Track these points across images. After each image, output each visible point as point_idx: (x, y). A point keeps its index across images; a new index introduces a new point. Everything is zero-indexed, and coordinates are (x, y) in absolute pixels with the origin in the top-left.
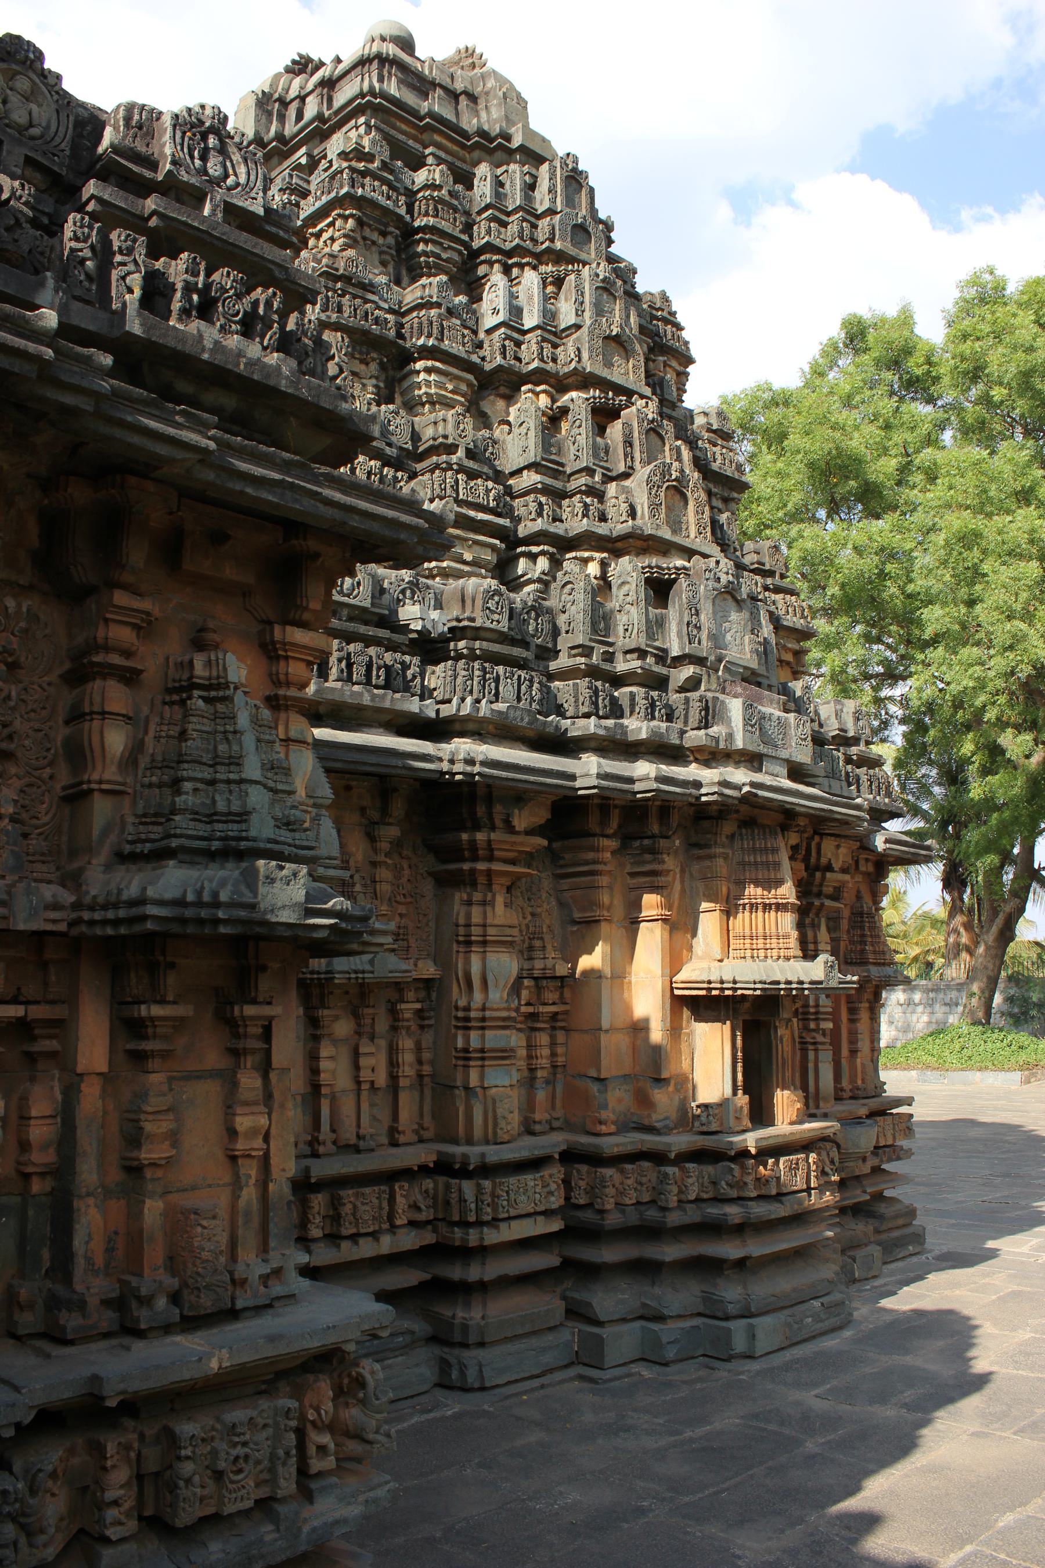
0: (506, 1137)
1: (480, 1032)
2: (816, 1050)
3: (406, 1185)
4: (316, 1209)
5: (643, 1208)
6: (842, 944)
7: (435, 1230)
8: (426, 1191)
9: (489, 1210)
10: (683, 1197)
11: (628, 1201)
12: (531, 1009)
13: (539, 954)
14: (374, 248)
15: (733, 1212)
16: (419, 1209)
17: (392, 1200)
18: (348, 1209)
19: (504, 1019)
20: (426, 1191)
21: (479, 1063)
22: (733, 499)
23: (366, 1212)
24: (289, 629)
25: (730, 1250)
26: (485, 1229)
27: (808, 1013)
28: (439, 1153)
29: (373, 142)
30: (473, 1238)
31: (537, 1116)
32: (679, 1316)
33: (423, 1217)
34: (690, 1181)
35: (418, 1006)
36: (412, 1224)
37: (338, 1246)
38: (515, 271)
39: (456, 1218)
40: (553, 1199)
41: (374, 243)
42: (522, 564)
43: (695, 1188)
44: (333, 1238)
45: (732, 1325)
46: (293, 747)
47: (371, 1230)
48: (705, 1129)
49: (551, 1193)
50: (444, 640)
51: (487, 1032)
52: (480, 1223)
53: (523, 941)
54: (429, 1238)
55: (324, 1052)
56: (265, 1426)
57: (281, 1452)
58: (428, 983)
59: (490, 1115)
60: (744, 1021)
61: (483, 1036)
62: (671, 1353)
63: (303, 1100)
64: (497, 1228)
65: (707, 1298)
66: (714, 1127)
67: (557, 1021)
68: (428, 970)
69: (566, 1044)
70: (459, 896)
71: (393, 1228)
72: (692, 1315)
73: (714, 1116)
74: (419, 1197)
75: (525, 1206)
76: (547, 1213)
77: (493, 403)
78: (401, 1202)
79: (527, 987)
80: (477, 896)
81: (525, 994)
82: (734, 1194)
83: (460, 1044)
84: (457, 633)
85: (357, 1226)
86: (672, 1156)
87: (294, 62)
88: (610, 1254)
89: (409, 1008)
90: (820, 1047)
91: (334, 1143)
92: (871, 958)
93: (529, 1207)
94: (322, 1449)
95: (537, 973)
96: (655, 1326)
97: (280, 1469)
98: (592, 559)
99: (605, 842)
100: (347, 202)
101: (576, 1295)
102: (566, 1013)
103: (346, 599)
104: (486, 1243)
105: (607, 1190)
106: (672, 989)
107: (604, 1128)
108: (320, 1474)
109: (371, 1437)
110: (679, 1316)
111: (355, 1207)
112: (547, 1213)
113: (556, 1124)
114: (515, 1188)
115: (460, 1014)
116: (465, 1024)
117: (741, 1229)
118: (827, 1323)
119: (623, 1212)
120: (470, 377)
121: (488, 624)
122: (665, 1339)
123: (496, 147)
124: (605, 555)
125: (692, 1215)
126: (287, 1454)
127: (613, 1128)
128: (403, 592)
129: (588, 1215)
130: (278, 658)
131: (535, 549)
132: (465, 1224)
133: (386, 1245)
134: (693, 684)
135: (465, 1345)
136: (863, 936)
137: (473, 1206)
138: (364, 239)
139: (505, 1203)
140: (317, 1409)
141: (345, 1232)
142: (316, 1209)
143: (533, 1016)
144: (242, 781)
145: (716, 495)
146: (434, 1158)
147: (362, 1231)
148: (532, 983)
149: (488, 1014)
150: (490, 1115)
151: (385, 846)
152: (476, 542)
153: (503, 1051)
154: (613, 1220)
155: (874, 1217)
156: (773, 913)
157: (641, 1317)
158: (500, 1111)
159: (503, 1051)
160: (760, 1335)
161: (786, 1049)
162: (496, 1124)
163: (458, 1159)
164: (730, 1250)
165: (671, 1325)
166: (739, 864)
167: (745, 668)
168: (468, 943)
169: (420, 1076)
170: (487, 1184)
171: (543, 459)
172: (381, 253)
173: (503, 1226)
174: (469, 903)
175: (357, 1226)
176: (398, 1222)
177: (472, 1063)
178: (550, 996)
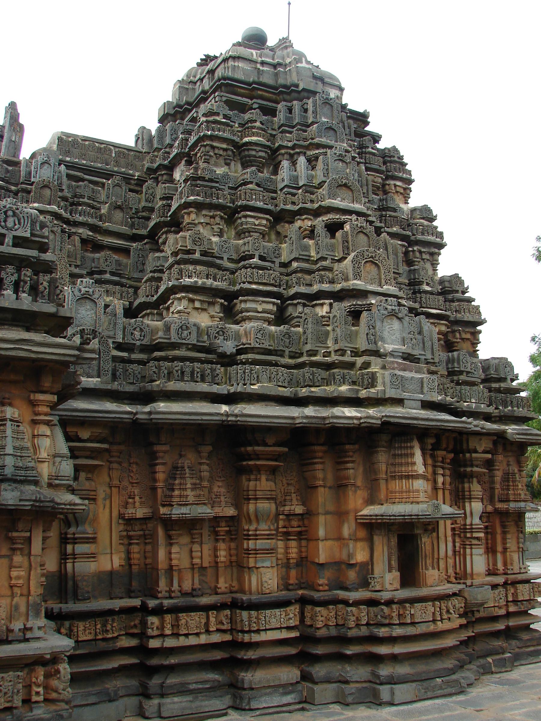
0: (268, 591)
1: (254, 541)
2: (471, 548)
3: (215, 612)
4: (168, 621)
5: (339, 627)
6: (496, 491)
7: (232, 634)
8: (227, 615)
9: (255, 625)
10: (359, 622)
11: (331, 624)
12: (285, 530)
13: (288, 503)
14: (221, 158)
15: (383, 632)
16: (223, 624)
17: (208, 618)
18: (183, 622)
19: (268, 535)
20: (227, 615)
21: (254, 556)
22: (436, 253)
23: (192, 624)
24: (37, 395)
25: (383, 650)
26: (252, 634)
27: (466, 529)
28: (233, 598)
29: (218, 107)
30: (247, 638)
31: (291, 582)
32: (357, 682)
33: (224, 627)
34: (363, 614)
35: (227, 529)
36: (218, 630)
37: (178, 639)
38: (295, 157)
39: (239, 628)
40: (291, 621)
41: (221, 155)
42: (290, 310)
43: (366, 618)
44: (176, 635)
45: (381, 687)
46: (41, 438)
47: (195, 632)
48: (373, 589)
49: (291, 619)
50: (232, 356)
51: (258, 541)
52: (249, 632)
53: (282, 497)
54: (228, 637)
55: (173, 550)
56: (10, 681)
57: (16, 691)
58: (232, 518)
59: (260, 580)
60: (398, 535)
61: (256, 543)
62: (350, 699)
63: (166, 572)
64: (259, 633)
65: (374, 674)
66: (377, 588)
67: (302, 535)
68: (231, 512)
69: (307, 547)
70: (244, 478)
71: (208, 632)
72: (365, 682)
73: (378, 582)
74: (224, 619)
75: (274, 623)
76: (289, 628)
77: (283, 227)
78: (212, 619)
79: (282, 519)
80: (252, 477)
81: (281, 523)
82: (387, 621)
83: (245, 546)
84: (240, 352)
85: (188, 630)
86: (351, 602)
87: (201, 60)
88: (320, 650)
89: (223, 528)
90: (473, 547)
91: (180, 591)
92: (511, 497)
93: (276, 626)
94: (38, 693)
95: (286, 512)
96: (343, 686)
97: (15, 697)
98: (325, 304)
99: (317, 448)
100: (205, 139)
101: (307, 669)
102: (306, 531)
103: (184, 341)
104: (252, 641)
105: (317, 618)
106: (356, 519)
107: (321, 588)
108: (36, 702)
109: (61, 691)
110: (357, 682)
111: (187, 621)
112: (289, 628)
113: (303, 586)
114: (269, 615)
115: (245, 533)
116: (248, 537)
117: (392, 640)
118: (445, 690)
119: (328, 629)
120: (268, 217)
121: (257, 346)
122: (347, 693)
123: (290, 92)
124: (332, 301)
125: (364, 631)
126: (18, 691)
127: (326, 588)
128: (218, 333)
129: (309, 630)
130: (35, 405)
131: (295, 302)
132: (243, 632)
133: (203, 639)
134: (366, 365)
135: (245, 689)
136: (508, 486)
137: (247, 623)
138: (216, 154)
139: (263, 622)
140: (37, 679)
141: (181, 633)
142: (168, 621)
143: (287, 534)
144: (5, 455)
145: (424, 252)
146: (230, 600)
147: (190, 632)
148: (284, 517)
149: (474, 527)
150: (260, 580)
151: (205, 454)
152: (263, 302)
153: (268, 550)
154: (322, 633)
155: (517, 639)
156: (411, 480)
157: (340, 682)
158: (264, 579)
159: (268, 550)
160: (397, 693)
161: (427, 548)
162: (262, 585)
163: (239, 601)
164: (383, 650)
165: (352, 685)
166: (393, 455)
167: (403, 353)
168: (249, 499)
169: (231, 562)
170: (254, 613)
171: (300, 255)
172: (225, 159)
173: (263, 633)
174: (250, 480)
175: (188, 630)
176: (211, 629)
177: (250, 556)
178: (295, 523)
